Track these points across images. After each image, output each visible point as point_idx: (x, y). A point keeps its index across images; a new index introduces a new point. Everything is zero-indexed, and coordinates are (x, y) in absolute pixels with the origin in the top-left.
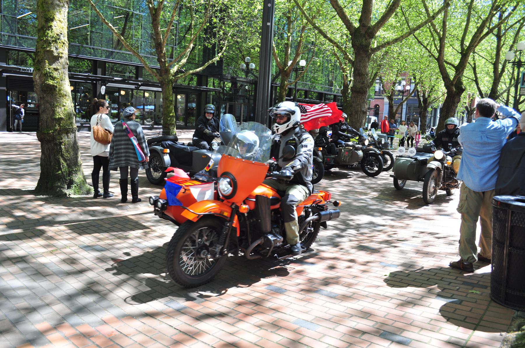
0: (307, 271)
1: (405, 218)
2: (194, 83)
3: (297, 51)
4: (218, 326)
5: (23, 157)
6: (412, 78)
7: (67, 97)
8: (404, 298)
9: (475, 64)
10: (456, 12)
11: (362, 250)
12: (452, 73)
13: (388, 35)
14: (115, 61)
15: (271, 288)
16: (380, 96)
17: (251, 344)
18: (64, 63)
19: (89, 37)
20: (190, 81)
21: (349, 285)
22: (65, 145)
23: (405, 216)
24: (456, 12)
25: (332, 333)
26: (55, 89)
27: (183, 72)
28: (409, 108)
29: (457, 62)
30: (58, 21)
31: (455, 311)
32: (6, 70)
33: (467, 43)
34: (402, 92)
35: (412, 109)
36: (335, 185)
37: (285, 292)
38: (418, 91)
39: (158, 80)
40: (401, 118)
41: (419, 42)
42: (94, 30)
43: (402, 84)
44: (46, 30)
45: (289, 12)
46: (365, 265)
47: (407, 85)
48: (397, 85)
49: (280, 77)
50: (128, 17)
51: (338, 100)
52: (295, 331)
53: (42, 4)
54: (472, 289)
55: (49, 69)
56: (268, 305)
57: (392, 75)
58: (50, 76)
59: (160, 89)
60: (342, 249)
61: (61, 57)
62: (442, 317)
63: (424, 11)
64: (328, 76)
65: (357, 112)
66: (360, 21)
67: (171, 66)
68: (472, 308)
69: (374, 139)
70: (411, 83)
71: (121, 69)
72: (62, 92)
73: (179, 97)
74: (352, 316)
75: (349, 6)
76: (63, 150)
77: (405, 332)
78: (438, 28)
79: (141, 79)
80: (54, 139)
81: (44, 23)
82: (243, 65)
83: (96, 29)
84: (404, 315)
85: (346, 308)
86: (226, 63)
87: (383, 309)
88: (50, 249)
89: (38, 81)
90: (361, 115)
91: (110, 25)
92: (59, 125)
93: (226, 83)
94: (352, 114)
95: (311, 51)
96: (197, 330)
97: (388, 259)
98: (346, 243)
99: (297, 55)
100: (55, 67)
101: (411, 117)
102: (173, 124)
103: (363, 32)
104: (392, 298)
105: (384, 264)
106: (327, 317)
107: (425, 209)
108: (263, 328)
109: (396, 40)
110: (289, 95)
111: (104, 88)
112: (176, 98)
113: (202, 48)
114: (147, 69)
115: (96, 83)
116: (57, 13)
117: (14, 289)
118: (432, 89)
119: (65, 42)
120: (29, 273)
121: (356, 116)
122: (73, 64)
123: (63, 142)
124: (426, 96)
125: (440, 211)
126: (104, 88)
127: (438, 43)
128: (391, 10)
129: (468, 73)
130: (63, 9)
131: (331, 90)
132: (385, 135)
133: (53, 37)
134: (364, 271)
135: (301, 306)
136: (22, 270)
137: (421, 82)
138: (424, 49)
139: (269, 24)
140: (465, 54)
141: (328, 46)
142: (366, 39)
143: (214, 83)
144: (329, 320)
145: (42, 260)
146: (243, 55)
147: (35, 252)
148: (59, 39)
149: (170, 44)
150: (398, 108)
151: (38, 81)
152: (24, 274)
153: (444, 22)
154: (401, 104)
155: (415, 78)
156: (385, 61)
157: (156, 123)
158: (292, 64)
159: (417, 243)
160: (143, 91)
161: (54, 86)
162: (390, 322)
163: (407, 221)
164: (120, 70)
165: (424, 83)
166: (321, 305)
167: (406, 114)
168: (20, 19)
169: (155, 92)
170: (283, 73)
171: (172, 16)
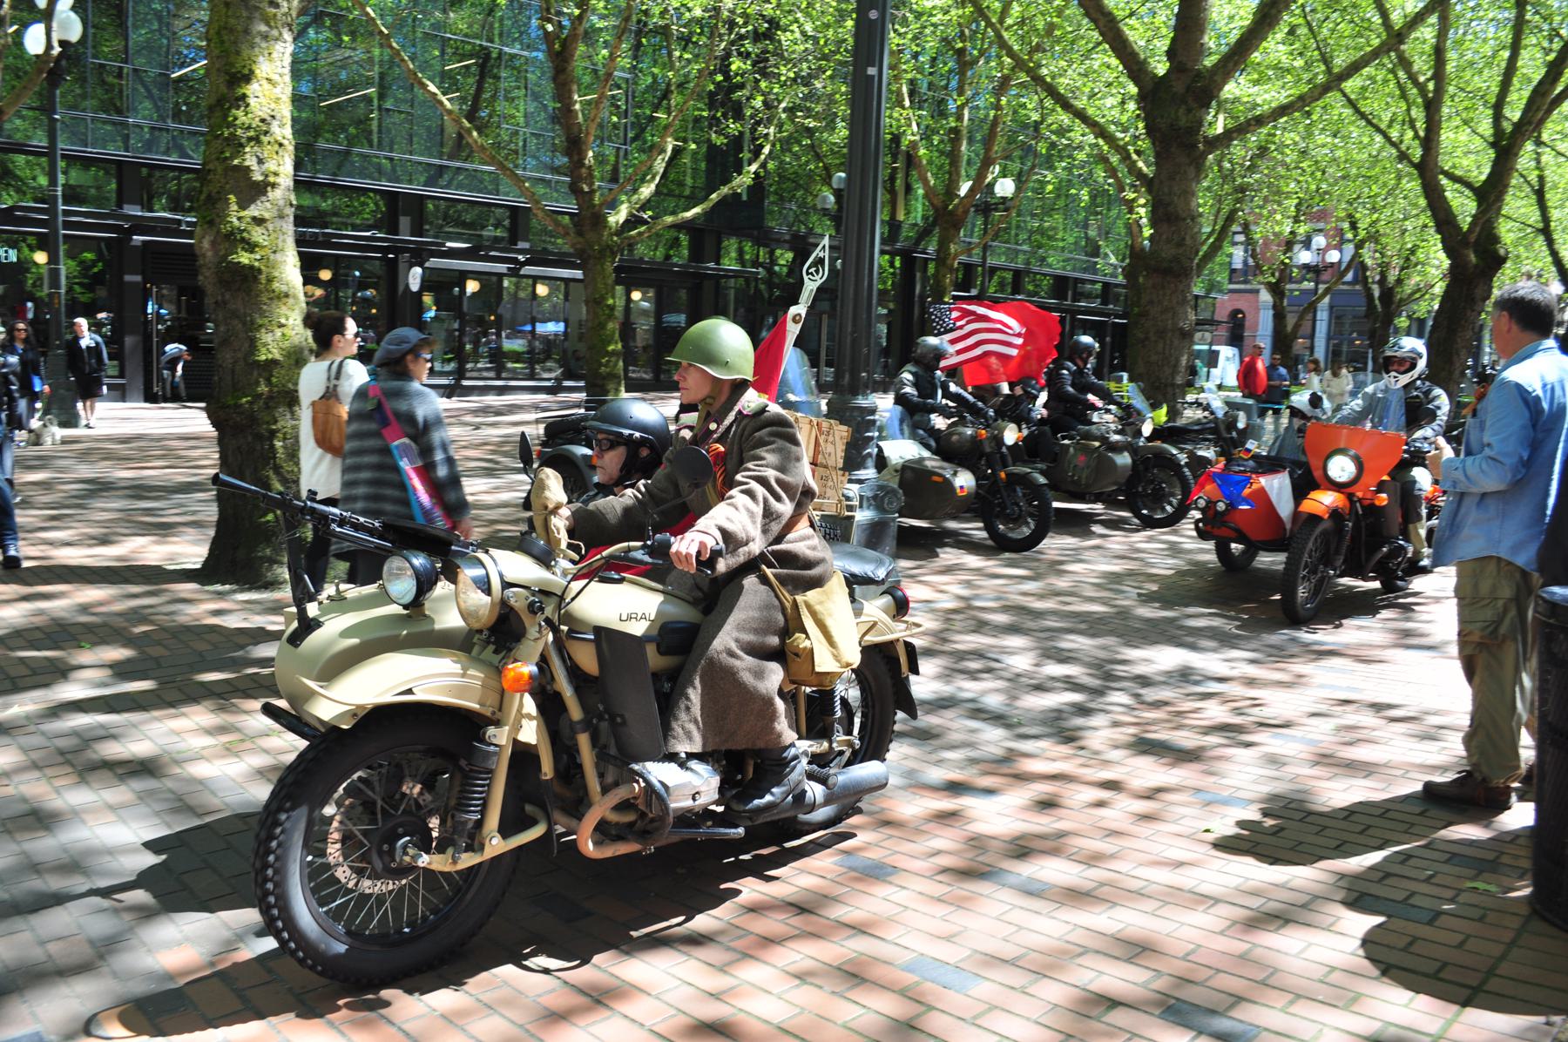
0: (970, 813)
1: (1292, 656)
2: (682, 256)
3: (988, 149)
4: (674, 971)
5: (180, 476)
6: (1346, 226)
7: (291, 301)
8: (1255, 903)
9: (1541, 179)
10: (1481, 19)
11: (1144, 752)
12: (1464, 206)
13: (1268, 97)
14: (452, 193)
15: (852, 861)
16: (1246, 282)
17: (847, 1032)
18: (281, 203)
19: (374, 126)
20: (671, 248)
21: (1094, 859)
22: (285, 439)
23: (1295, 650)
24: (1481, 19)
25: (1020, 1004)
26: (256, 280)
27: (645, 222)
28: (1336, 317)
29: (1481, 174)
30: (264, 82)
31: (1411, 944)
32: (140, 226)
33: (1514, 113)
34: (1313, 270)
35: (1348, 321)
36: (1086, 555)
37: (890, 874)
38: (1363, 267)
39: (573, 246)
40: (1312, 349)
41: (1363, 116)
42: (388, 105)
43: (1314, 246)
44: (229, 109)
45: (962, 36)
46: (1148, 798)
47: (1329, 247)
48: (1297, 247)
49: (937, 230)
50: (486, 65)
51: (1117, 295)
52: (905, 993)
53: (218, 33)
54: (1474, 879)
55: (239, 219)
56: (839, 912)
57: (1278, 217)
58: (243, 240)
59: (578, 274)
60: (1082, 748)
61: (274, 185)
62: (1366, 963)
63: (1377, 20)
64: (1086, 226)
65: (1161, 333)
66: (1171, 54)
67: (613, 205)
68: (1468, 936)
69: (1212, 413)
70: (1343, 241)
71: (459, 217)
72: (276, 285)
73: (636, 295)
74: (1085, 951)
75: (1143, 10)
76: (281, 454)
77: (1244, 1004)
78: (1422, 65)
79: (526, 245)
80: (253, 420)
81: (224, 89)
82: (825, 198)
83: (396, 100)
84: (1246, 953)
85: (1070, 927)
86: (776, 193)
87: (1187, 933)
88: (225, 738)
89: (209, 254)
90: (1176, 342)
91: (432, 88)
92: (269, 382)
93: (778, 252)
94: (1147, 338)
95: (1025, 149)
96: (613, 980)
97: (1224, 781)
98: (1099, 733)
99: (987, 163)
100: (256, 214)
101: (1345, 348)
102: (616, 377)
103: (1179, 87)
104: (1217, 901)
105: (1208, 797)
106: (1009, 951)
107: (1360, 628)
108: (810, 980)
109: (1283, 110)
110: (965, 285)
111: (417, 271)
112: (629, 300)
113: (704, 149)
114: (540, 214)
115: (395, 260)
116: (261, 59)
117: (111, 852)
118: (1408, 259)
119: (286, 142)
120: (158, 807)
121: (1161, 345)
122: (307, 201)
123: (278, 431)
124: (1392, 276)
125: (1407, 633)
126: (417, 271)
127: (1418, 114)
128: (1265, 20)
129: (1517, 206)
130: (279, 46)
131: (1092, 268)
132: (1250, 402)
133: (249, 128)
134: (1147, 817)
135: (935, 918)
136: (142, 797)
137: (1374, 237)
138: (1379, 138)
139: (872, 71)
140: (1505, 147)
141: (1080, 133)
142: (1189, 111)
143: (741, 252)
144: (1012, 963)
145: (200, 770)
146: (826, 168)
147: (181, 746)
148: (266, 133)
149: (610, 140)
150: (1301, 318)
151: (209, 254)
152: (143, 809)
153: (1439, 53)
154: (1312, 308)
155: (1354, 226)
156: (1257, 176)
157: (569, 375)
158: (972, 190)
159: (1322, 732)
160: (530, 281)
161: (252, 267)
162: (1203, 974)
163: (1299, 667)
164: (468, 218)
165: (1384, 240)
166: (1000, 917)
167: (1329, 338)
168: (180, 79)
169: (567, 281)
170: (945, 218)
171: (612, 57)
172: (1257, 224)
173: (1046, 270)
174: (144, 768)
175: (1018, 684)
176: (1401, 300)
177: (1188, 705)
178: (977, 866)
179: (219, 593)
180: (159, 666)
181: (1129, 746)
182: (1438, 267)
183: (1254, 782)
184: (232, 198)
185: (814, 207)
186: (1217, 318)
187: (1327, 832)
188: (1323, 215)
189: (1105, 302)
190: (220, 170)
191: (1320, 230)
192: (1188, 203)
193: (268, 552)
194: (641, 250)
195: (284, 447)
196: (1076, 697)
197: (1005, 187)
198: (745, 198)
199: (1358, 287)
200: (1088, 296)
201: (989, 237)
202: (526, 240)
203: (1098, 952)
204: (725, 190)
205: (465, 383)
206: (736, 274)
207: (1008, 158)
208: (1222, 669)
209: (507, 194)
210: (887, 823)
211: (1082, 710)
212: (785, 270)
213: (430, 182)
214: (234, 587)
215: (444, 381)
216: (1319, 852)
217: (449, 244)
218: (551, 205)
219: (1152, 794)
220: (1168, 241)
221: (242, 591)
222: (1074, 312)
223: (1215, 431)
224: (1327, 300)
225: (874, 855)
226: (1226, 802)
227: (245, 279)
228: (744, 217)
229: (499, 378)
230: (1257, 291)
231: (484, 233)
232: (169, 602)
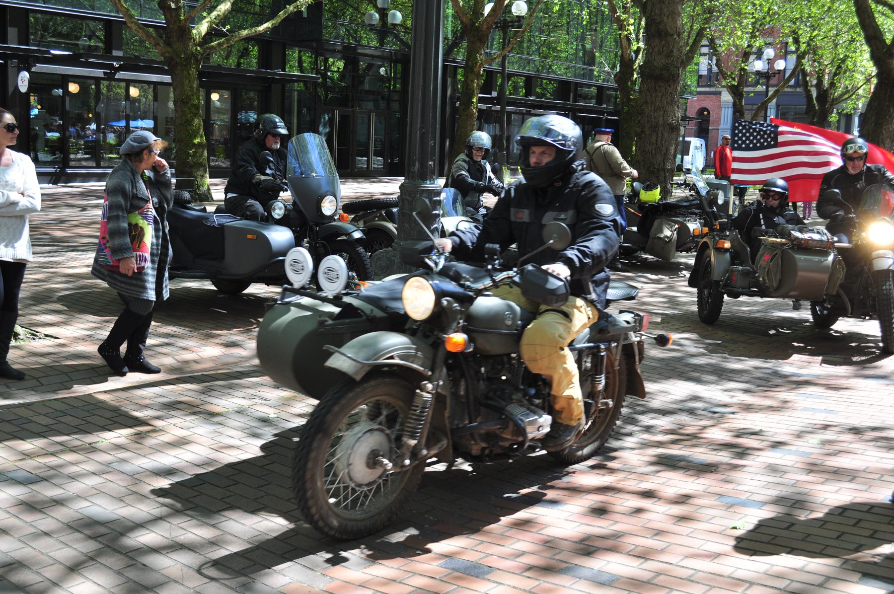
0: (542, 520)
1: (777, 386)
2: (253, 61)
6: (790, 40)
21: (643, 555)
23: (779, 381)
27: (223, 35)
37: (488, 573)
43: (765, 57)
49: (465, 44)
51: (609, 98)
57: (739, 33)
59: (167, 79)
64: (582, 38)
65: (654, 128)
69: (698, 192)
70: (787, 53)
71: (68, 29)
73: (215, 97)
82: (371, 16)
90: (666, 135)
94: (643, 132)
97: (739, 488)
102: (201, 165)
105: (729, 500)
111: (25, 76)
112: (208, 99)
114: (134, 27)
121: (654, 138)
126: (25, 76)
134: (683, 519)
137: (813, 49)
143: (300, 62)
155: (796, 41)
158: (493, 10)
159: (811, 445)
164: (65, 30)
165: (820, 52)
169: (156, 84)
172: (720, 38)
173: (552, 76)
176: (833, 100)
182: (863, 73)
183: (764, 487)
185: (363, 25)
186: (688, 115)
188: (771, 32)
189: (599, 102)
191: (770, 44)
192: (675, 22)
194: (215, 59)
198: (305, 15)
200: (585, 97)
201: (508, 49)
202: (121, 49)
205: (69, 171)
206: (299, 79)
208: (725, 398)
209: (110, 11)
212: (336, 75)
215: (52, 170)
216: (887, 537)
217: (53, 52)
218: (146, 19)
219: (683, 499)
220: (660, 53)
223: (700, 206)
224: (774, 101)
226: (745, 504)
229: (98, 167)
230: (720, 93)
231: (80, 43)
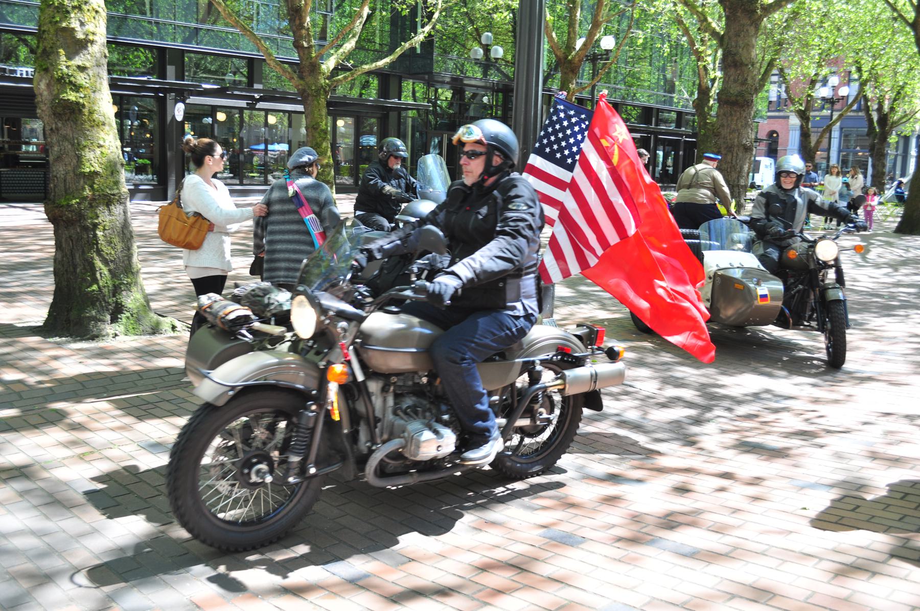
1: (842, 381)
2: (372, 94)
6: (853, 69)
7: (107, 128)
21: (719, 530)
22: (104, 229)
26: (80, 111)
28: (845, 136)
34: (831, 102)
35: (853, 138)
37: (581, 543)
38: (866, 99)
40: (828, 159)
43: (830, 84)
48: (818, 85)
51: (687, 122)
55: (67, 67)
56: (545, 570)
57: (807, 63)
58: (71, 82)
59: (300, 108)
61: (92, 42)
64: (664, 69)
70: (850, 81)
72: (95, 116)
73: (340, 123)
80: (81, 216)
82: (476, 51)
85: (718, 580)
88: (79, 451)
89: (45, 93)
90: (740, 155)
93: (440, 91)
98: (711, 435)
99: (596, 25)
100: (80, 63)
101: (851, 158)
114: (272, 64)
115: (165, 98)
119: (100, 10)
120: (35, 502)
134: (756, 499)
136: (22, 494)
137: (875, 77)
145: (60, 474)
150: (821, 137)
151: (45, 93)
152: (25, 504)
154: (829, 129)
155: (859, 70)
158: (585, 45)
159: (873, 437)
160: (263, 113)
161: (78, 103)
167: (840, 151)
169: (290, 113)
173: (636, 103)
174: (20, 473)
175: (647, 401)
176: (893, 123)
177: (771, 417)
178: (639, 534)
179: (58, 343)
180: (21, 398)
181: (735, 447)
184: (62, 51)
187: (891, 509)
188: (836, 62)
189: (679, 125)
190: (52, 31)
193: (94, 313)
195: (105, 236)
196: (692, 412)
197: (608, 43)
198: (419, 51)
199: (860, 114)
202: (261, 83)
203: (741, 597)
204: (407, 45)
207: (609, 21)
210: (573, 505)
211: (697, 421)
213: (186, 41)
214: (69, 339)
219: (756, 481)
221: (75, 342)
222: (657, 134)
224: (838, 124)
225: (566, 528)
227: (73, 112)
228: (418, 65)
229: (241, 184)
231: (226, 78)
232: (22, 351)
